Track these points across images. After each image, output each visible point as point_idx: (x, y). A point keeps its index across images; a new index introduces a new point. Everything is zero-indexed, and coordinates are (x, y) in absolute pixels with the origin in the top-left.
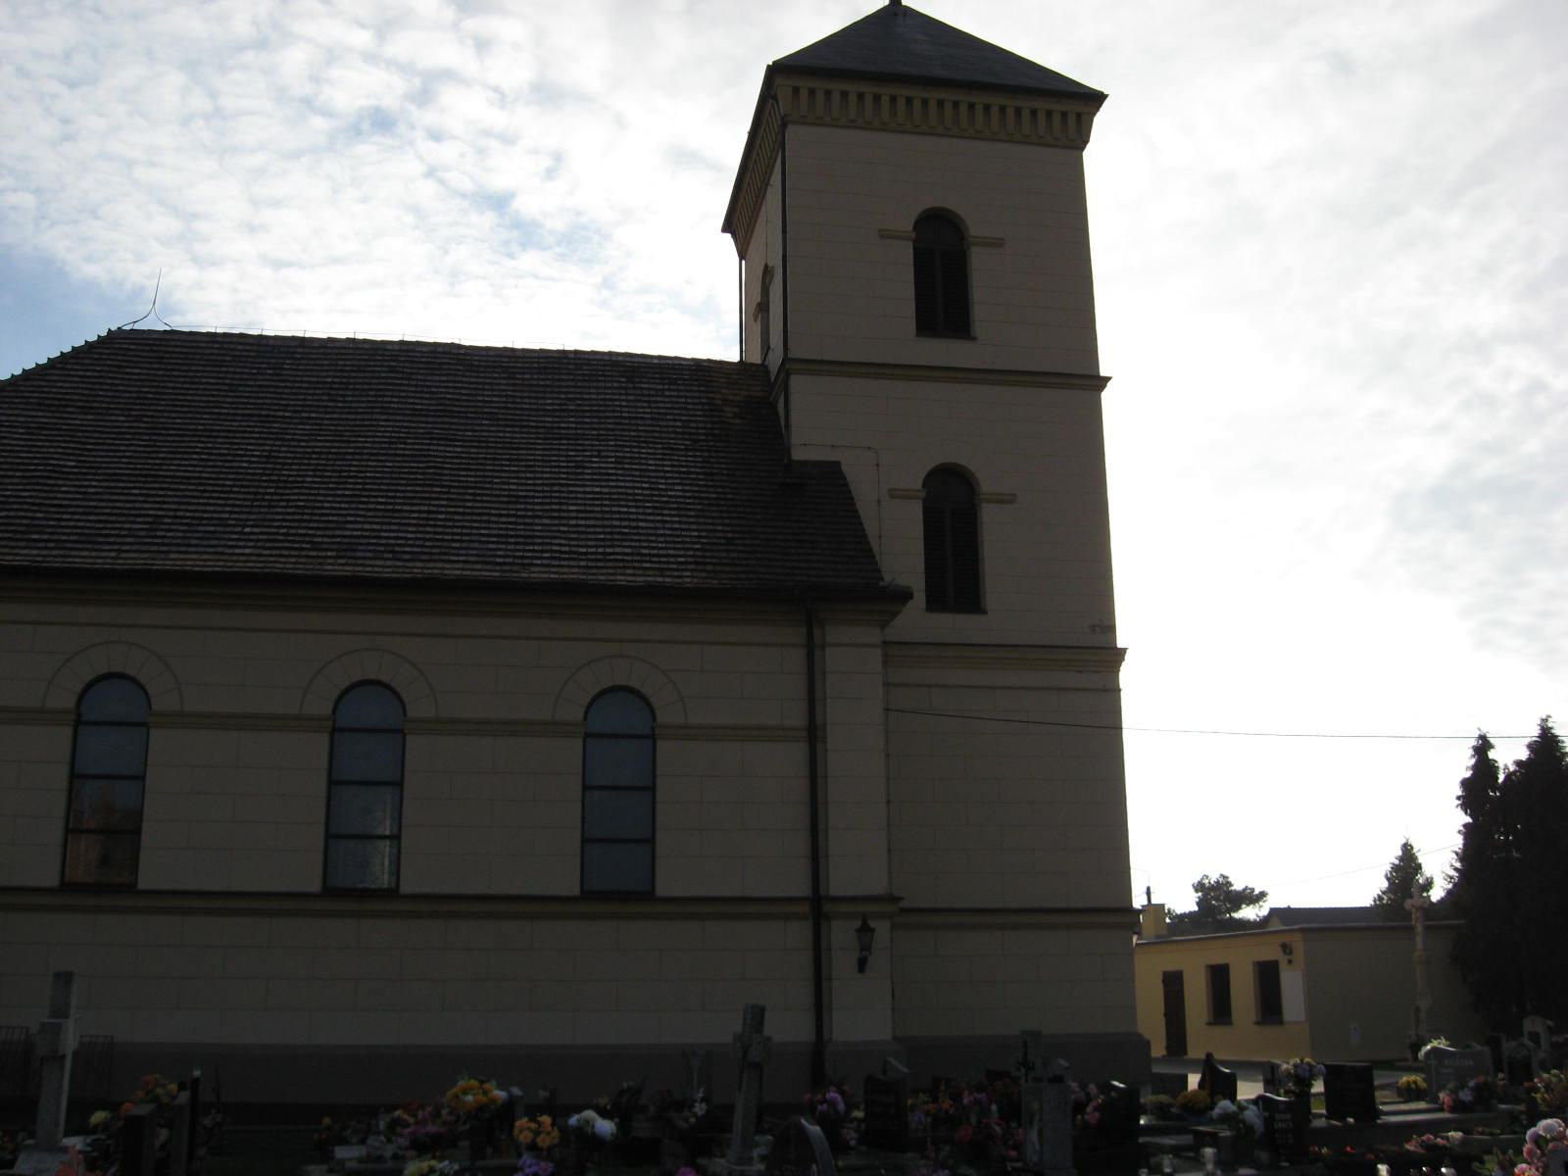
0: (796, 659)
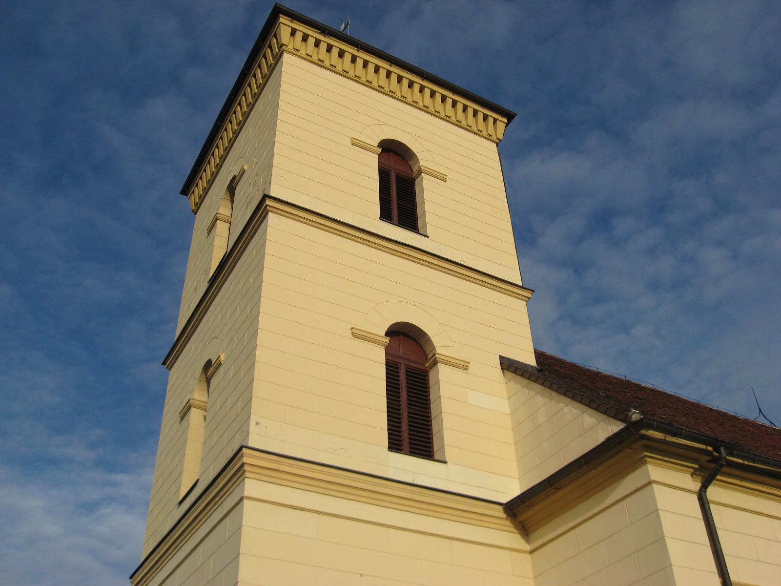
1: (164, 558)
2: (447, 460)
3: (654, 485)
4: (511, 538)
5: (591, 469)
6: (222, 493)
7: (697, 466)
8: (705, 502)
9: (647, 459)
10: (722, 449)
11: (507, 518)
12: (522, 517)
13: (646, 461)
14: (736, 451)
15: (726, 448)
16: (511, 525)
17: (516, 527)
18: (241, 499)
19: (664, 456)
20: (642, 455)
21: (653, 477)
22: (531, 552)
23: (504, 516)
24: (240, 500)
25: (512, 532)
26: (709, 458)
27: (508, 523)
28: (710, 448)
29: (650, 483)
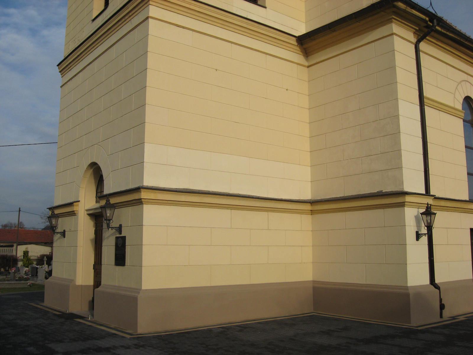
0: (412, 49)
1: (84, 54)
2: (267, 6)
3: (395, 36)
4: (297, 57)
5: (358, 22)
6: (130, 14)
7: (418, 29)
8: (418, 50)
9: (393, 20)
10: (435, 21)
11: (297, 45)
12: (305, 46)
13: (392, 21)
14: (441, 23)
15: (437, 20)
16: (299, 50)
17: (301, 52)
18: (147, 18)
19: (402, 19)
20: (391, 17)
21: (394, 31)
22: (308, 67)
23: (296, 44)
24: (146, 18)
25: (299, 54)
26: (425, 25)
27: (298, 48)
28: (427, 19)
29: (392, 34)
